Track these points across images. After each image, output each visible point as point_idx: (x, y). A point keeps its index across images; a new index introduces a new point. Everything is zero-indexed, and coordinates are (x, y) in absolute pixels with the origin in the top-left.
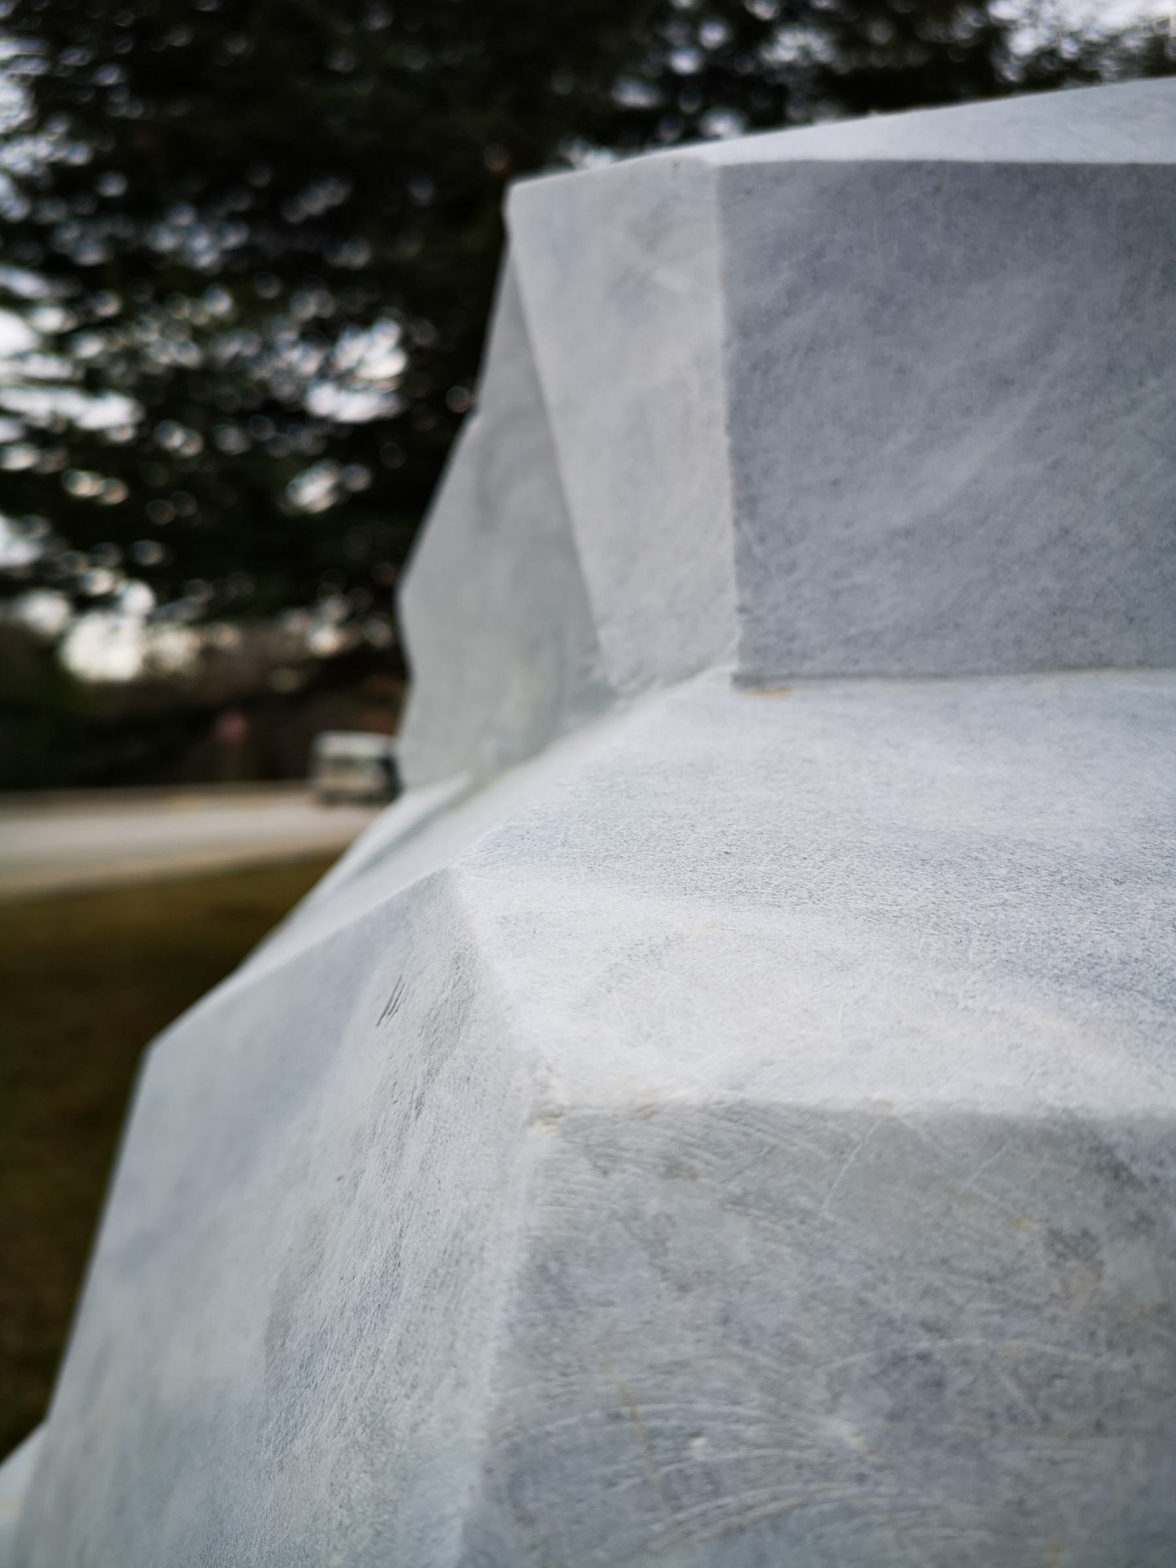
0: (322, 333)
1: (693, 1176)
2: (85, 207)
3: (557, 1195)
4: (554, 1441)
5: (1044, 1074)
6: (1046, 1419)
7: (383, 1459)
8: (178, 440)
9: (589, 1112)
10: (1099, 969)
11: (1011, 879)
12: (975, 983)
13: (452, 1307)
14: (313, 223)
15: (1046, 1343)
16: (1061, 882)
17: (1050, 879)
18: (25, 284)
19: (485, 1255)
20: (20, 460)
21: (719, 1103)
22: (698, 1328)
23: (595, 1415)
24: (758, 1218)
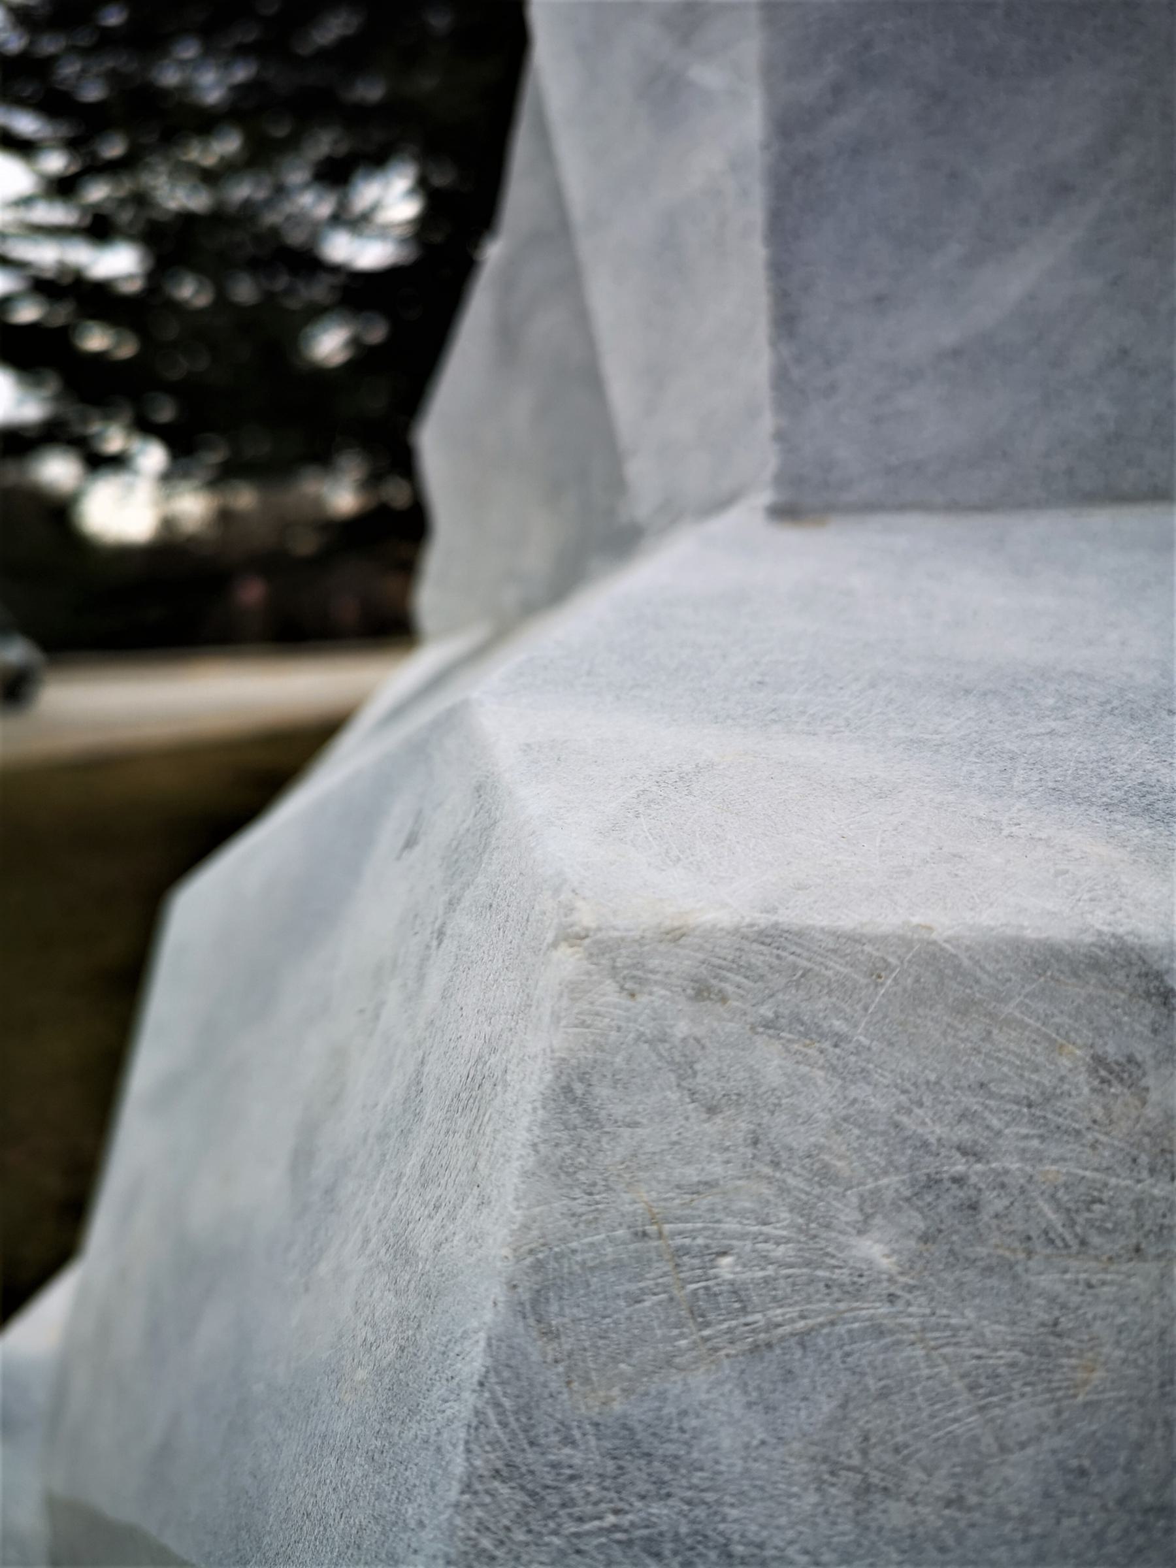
0: (336, 174)
1: (724, 999)
2: (85, 39)
3: (582, 1017)
4: (579, 1258)
5: (1092, 900)
6: (1083, 1243)
7: (407, 1278)
8: (189, 291)
9: (616, 934)
10: (1151, 798)
11: (1058, 708)
12: (1020, 810)
13: (476, 1128)
14: (325, 55)
15: (1086, 1169)
16: (1111, 712)
17: (1099, 709)
18: (26, 124)
19: (508, 1078)
20: (27, 313)
21: (751, 925)
22: (727, 1149)
23: (620, 1232)
24: (789, 1041)
